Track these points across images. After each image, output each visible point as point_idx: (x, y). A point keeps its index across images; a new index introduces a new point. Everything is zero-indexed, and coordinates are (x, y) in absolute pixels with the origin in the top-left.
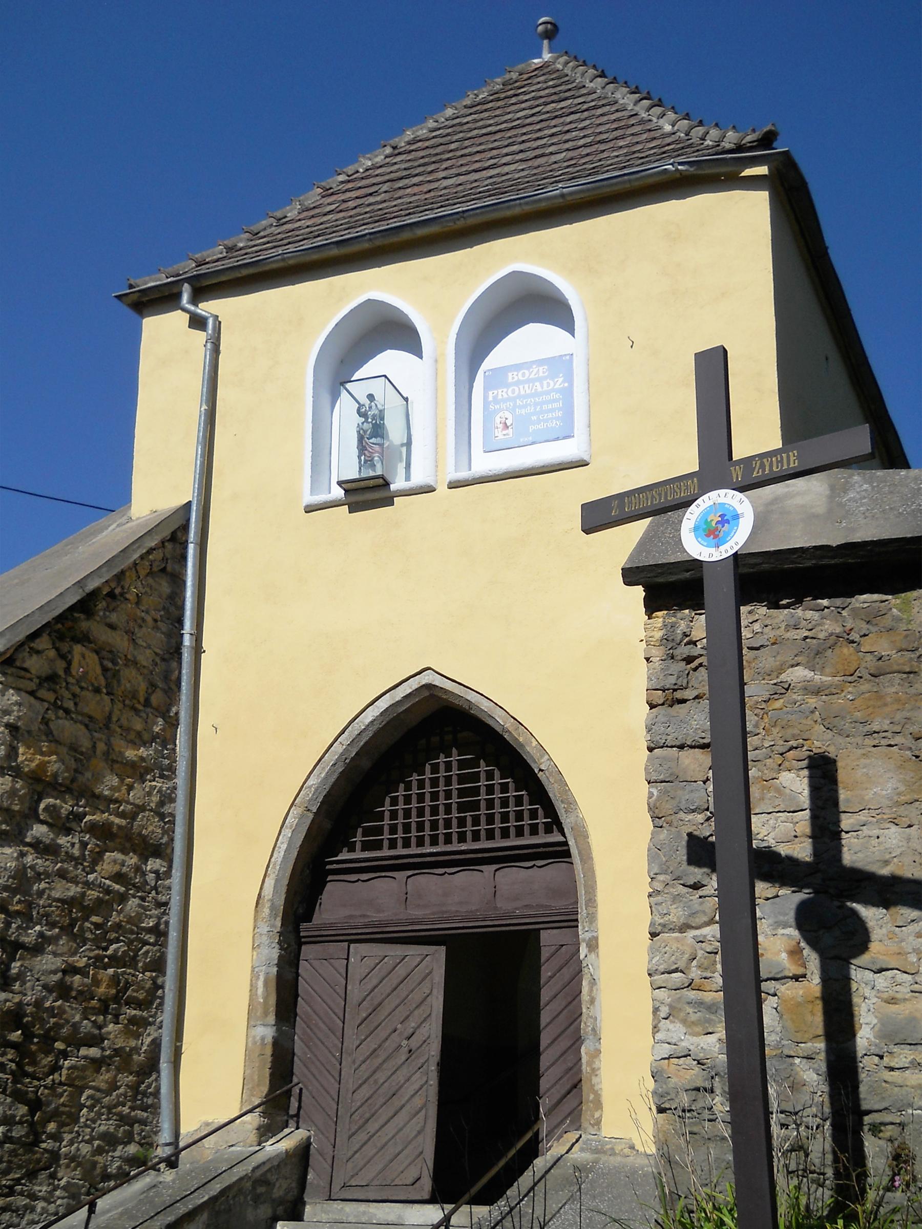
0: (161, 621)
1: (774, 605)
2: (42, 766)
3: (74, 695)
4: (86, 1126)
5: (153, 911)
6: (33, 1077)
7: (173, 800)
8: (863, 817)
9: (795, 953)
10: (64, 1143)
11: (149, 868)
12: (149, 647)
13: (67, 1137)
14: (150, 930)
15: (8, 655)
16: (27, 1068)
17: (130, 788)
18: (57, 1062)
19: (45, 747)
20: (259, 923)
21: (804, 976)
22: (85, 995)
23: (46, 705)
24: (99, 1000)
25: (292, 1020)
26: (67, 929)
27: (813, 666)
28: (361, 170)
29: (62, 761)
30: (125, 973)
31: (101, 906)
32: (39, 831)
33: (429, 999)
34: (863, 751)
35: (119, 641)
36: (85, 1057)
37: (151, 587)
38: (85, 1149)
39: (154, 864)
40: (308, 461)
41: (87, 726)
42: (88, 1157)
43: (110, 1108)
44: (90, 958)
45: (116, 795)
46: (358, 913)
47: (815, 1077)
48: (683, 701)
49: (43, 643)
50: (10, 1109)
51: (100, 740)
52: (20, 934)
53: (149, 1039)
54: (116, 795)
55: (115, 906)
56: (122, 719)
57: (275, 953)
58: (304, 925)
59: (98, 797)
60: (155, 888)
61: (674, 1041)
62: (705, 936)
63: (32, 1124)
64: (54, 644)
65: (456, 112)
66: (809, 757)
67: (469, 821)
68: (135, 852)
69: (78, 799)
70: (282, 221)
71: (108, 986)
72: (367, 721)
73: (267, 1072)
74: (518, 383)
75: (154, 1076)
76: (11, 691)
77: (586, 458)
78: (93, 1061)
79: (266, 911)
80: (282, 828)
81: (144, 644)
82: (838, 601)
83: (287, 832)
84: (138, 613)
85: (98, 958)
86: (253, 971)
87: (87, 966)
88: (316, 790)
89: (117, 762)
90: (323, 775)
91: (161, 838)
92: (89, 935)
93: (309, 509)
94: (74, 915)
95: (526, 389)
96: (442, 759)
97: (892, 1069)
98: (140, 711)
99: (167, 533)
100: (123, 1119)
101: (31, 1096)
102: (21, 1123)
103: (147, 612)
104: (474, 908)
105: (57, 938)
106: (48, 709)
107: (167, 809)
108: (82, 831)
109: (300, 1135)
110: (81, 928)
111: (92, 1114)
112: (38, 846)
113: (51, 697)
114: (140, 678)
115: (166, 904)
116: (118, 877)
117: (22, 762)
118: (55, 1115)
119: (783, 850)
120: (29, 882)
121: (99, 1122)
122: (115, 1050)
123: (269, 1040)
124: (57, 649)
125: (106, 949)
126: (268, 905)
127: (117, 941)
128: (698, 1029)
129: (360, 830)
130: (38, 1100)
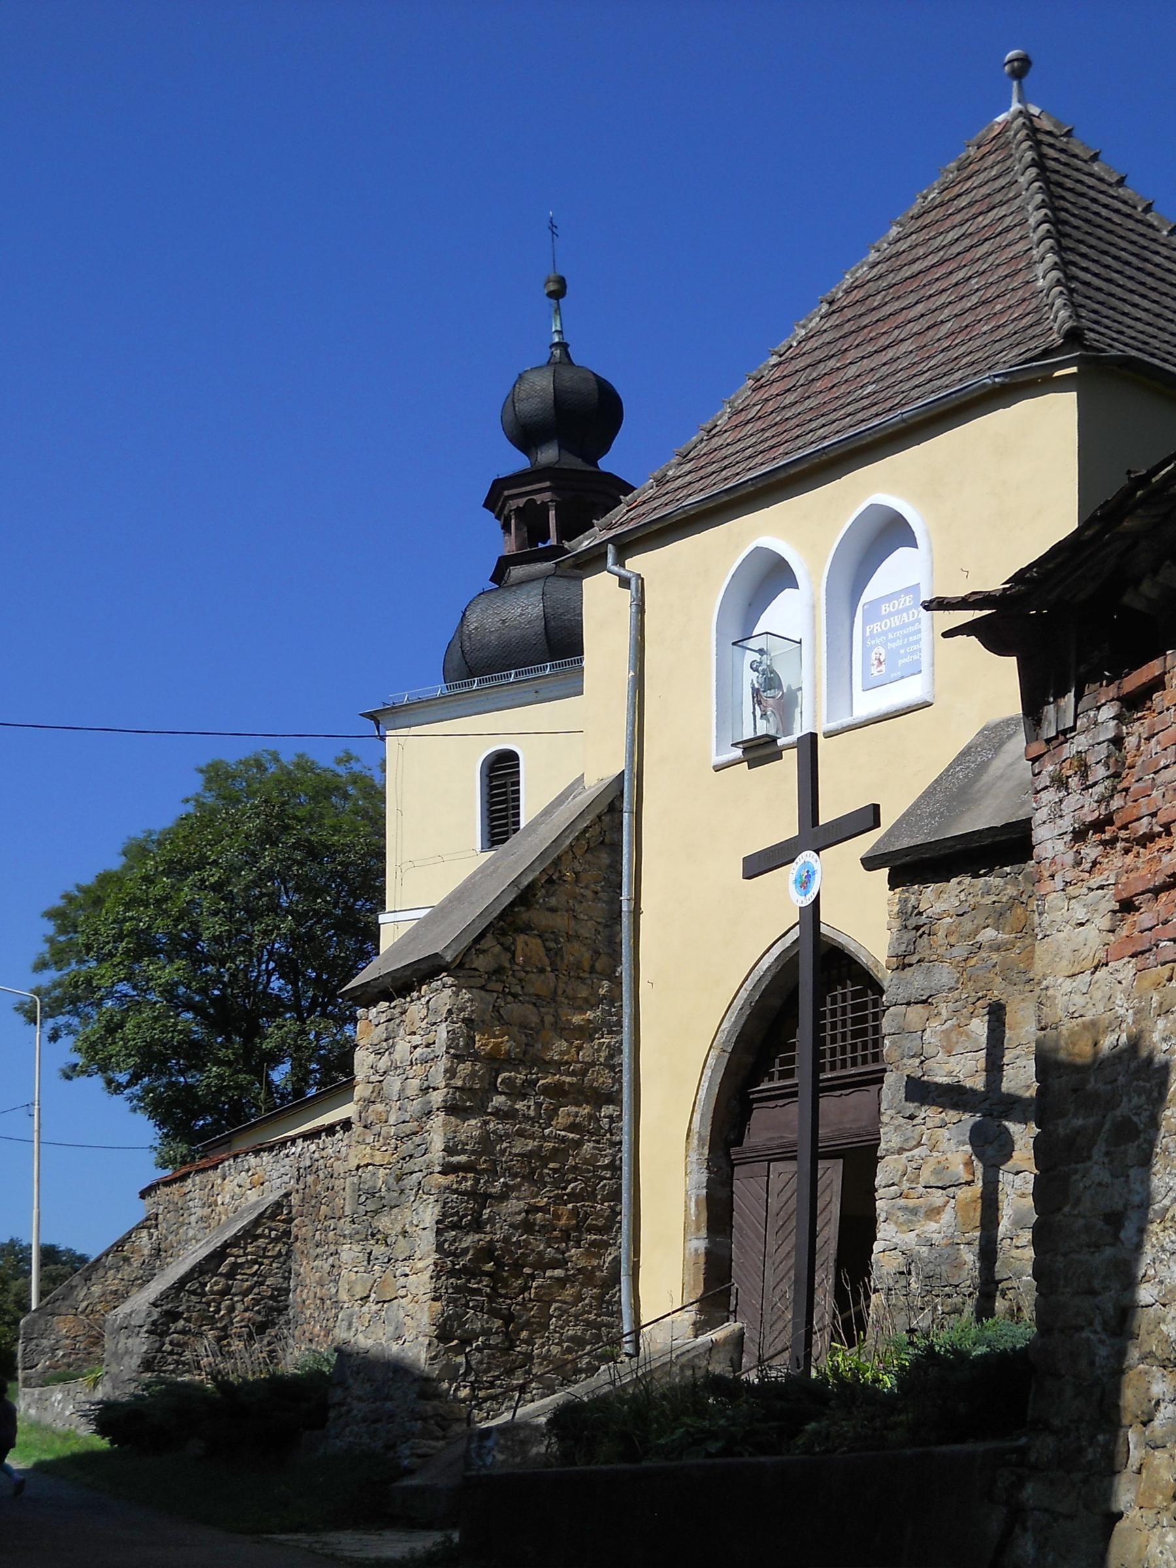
0: (604, 891)
1: (976, 876)
2: (497, 1046)
3: (521, 980)
4: (555, 1332)
5: (608, 1151)
6: (506, 1297)
7: (621, 1052)
8: (1017, 1052)
9: (968, 1164)
10: (536, 1346)
11: (602, 1114)
12: (591, 918)
13: (539, 1341)
14: (605, 1167)
15: (458, 961)
16: (500, 1291)
17: (579, 1048)
18: (526, 1284)
19: (497, 1030)
20: (691, 1153)
21: (973, 1181)
22: (547, 1228)
23: (495, 995)
24: (561, 1230)
25: (728, 1232)
26: (528, 1177)
27: (998, 926)
28: (795, 344)
29: (511, 1038)
30: (583, 1206)
31: (555, 1154)
32: (498, 1100)
33: (829, 1207)
34: (1022, 997)
35: (560, 921)
36: (550, 1278)
37: (589, 863)
38: (555, 1350)
39: (607, 1110)
40: (714, 721)
41: (534, 1004)
42: (558, 1355)
43: (576, 1317)
44: (550, 1198)
45: (566, 1058)
46: (776, 1135)
47: (972, 1257)
48: (911, 965)
49: (489, 942)
50: (487, 1323)
51: (548, 1013)
52: (488, 1187)
53: (610, 1258)
54: (566, 1058)
55: (571, 1152)
56: (567, 990)
57: (704, 1177)
58: (733, 1150)
59: (551, 1062)
60: (610, 1130)
61: (888, 1238)
62: (913, 1156)
63: (507, 1334)
64: (498, 939)
65: (901, 229)
66: (990, 1004)
67: (860, 1046)
68: (588, 1103)
69: (531, 1068)
70: (714, 432)
71: (568, 1219)
72: (764, 968)
73: (702, 1277)
74: (890, 615)
75: (617, 1288)
76: (464, 991)
77: (929, 700)
78: (558, 1279)
79: (695, 1142)
80: (704, 1068)
81: (586, 918)
82: (1016, 867)
83: (708, 1072)
84: (577, 890)
85: (558, 1197)
86: (686, 1194)
87: (548, 1204)
88: (729, 1032)
89: (566, 1029)
90: (733, 1019)
91: (612, 1087)
92: (547, 1179)
93: (718, 768)
94: (533, 1165)
95: (895, 622)
96: (840, 991)
97: (1018, 1247)
98: (585, 979)
99: (602, 807)
100: (589, 1324)
101: (505, 1312)
102: (497, 1333)
103: (586, 887)
104: (864, 1124)
105: (520, 1185)
106: (498, 998)
107: (616, 1061)
108: (537, 1094)
109: (739, 1325)
110: (541, 1174)
111: (561, 1322)
112: (498, 1114)
113: (499, 987)
114: (584, 949)
115: (620, 1143)
116: (572, 1127)
117: (479, 1048)
118: (527, 1325)
119: (968, 1083)
120: (493, 1144)
121: (567, 1328)
122: (578, 1269)
123: (702, 1250)
124: (502, 944)
125: (565, 1188)
126: (696, 1137)
127: (576, 1180)
128: (905, 1228)
129: (777, 1060)
130: (511, 1314)
